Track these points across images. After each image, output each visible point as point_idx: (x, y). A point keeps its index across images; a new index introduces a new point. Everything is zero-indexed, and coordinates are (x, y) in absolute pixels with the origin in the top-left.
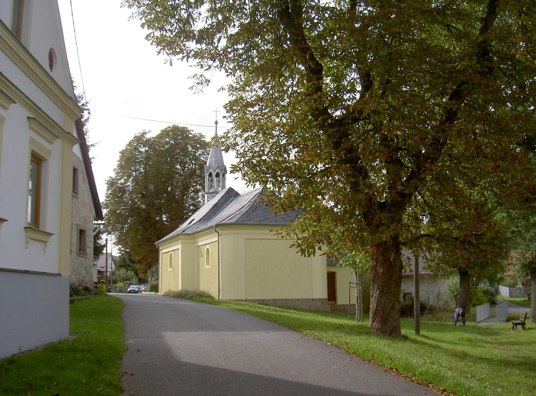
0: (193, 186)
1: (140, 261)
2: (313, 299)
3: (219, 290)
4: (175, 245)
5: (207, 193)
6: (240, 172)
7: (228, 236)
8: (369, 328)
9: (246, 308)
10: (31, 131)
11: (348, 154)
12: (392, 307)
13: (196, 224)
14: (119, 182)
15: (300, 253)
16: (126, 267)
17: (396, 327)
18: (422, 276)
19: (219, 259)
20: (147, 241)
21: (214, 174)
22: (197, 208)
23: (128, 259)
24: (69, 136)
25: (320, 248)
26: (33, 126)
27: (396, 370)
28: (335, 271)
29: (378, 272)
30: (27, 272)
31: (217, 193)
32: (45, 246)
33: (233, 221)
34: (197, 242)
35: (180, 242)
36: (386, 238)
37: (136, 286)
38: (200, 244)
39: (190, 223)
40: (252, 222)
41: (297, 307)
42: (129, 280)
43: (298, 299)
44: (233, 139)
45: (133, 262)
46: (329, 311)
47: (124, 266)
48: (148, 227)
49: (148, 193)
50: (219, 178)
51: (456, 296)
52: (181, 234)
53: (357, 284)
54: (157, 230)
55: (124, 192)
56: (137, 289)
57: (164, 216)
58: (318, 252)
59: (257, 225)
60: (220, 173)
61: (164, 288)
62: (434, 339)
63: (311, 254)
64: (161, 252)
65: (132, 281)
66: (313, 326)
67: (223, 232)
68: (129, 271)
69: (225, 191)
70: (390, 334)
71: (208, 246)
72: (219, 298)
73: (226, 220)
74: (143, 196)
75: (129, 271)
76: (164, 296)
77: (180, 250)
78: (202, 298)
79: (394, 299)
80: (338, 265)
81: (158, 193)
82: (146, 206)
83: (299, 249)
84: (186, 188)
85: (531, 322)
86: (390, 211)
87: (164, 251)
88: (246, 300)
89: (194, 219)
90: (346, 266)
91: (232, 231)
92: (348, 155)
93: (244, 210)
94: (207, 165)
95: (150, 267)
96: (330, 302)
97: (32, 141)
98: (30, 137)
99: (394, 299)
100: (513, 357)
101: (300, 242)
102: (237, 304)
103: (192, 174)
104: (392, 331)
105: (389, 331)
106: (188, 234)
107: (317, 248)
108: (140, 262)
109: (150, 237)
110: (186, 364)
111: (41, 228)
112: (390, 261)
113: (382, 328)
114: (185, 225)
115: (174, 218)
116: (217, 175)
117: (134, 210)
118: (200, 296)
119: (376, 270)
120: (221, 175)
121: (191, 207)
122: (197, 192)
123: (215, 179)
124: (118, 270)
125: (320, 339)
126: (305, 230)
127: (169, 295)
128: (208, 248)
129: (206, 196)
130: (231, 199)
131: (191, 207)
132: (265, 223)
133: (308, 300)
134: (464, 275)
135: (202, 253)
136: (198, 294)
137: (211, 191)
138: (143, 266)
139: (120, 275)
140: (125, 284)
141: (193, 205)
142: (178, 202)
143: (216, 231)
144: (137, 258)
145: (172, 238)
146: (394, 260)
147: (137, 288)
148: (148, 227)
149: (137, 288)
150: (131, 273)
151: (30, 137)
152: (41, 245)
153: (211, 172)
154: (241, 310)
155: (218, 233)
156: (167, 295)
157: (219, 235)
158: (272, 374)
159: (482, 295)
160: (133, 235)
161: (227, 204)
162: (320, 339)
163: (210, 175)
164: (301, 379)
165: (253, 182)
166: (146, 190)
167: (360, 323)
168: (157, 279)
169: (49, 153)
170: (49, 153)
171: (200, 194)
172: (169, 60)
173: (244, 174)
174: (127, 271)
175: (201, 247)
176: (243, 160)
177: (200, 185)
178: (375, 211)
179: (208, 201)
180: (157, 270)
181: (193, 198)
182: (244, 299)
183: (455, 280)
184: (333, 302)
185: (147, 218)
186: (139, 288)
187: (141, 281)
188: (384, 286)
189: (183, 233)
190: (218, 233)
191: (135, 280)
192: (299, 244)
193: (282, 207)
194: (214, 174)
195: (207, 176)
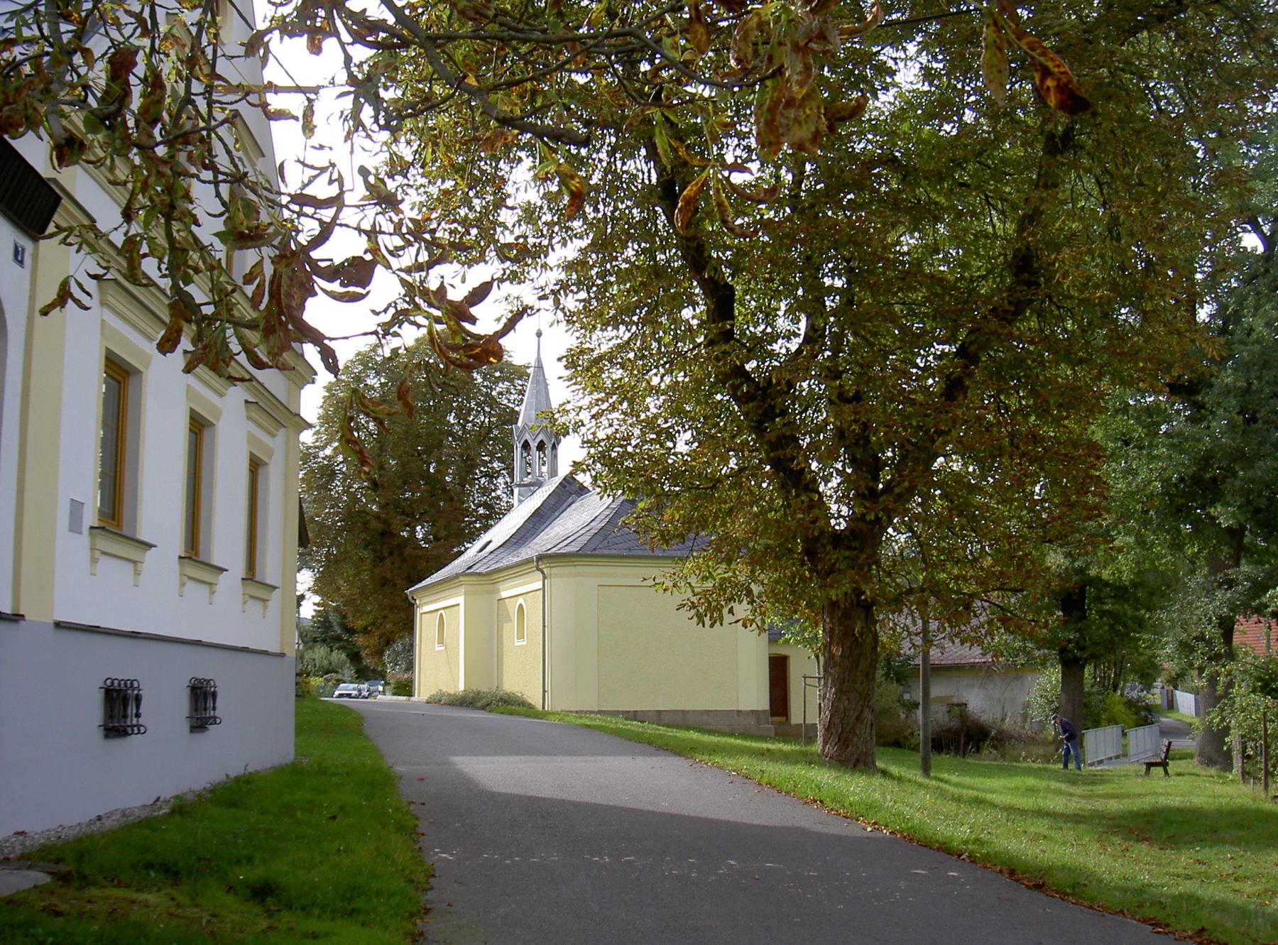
0: (485, 464)
1: (365, 628)
2: (739, 712)
3: (544, 691)
4: (450, 597)
5: (519, 486)
6: (588, 473)
7: (564, 580)
8: (818, 755)
9: (597, 723)
10: (250, 423)
11: (772, 451)
12: (858, 718)
13: (496, 553)
14: (321, 454)
15: (695, 619)
16: (328, 641)
17: (866, 754)
18: (989, 667)
19: (544, 626)
20: (384, 585)
21: (533, 445)
22: (494, 513)
23: (338, 623)
24: (297, 418)
25: (731, 611)
26: (253, 414)
27: (821, 801)
28: (787, 654)
29: (834, 655)
30: (245, 650)
31: (539, 484)
32: (265, 608)
33: (574, 548)
34: (499, 591)
35: (462, 589)
36: (837, 595)
37: (352, 686)
38: (504, 594)
39: (481, 550)
40: (615, 552)
41: (705, 727)
42: (336, 672)
43: (708, 712)
44: (574, 413)
45: (351, 631)
46: (773, 735)
47: (324, 641)
48: (386, 555)
49: (385, 479)
50: (544, 453)
51: (1056, 710)
52: (464, 574)
53: (819, 678)
54: (404, 560)
55: (332, 475)
56: (354, 693)
57: (418, 528)
58: (728, 618)
59: (623, 557)
60: (546, 441)
61: (425, 687)
62: (957, 785)
63: (715, 622)
64: (419, 611)
65: (343, 675)
66: (714, 750)
67: (554, 571)
68: (335, 653)
69: (557, 481)
70: (855, 766)
71: (521, 600)
72: (544, 708)
73: (559, 546)
74: (375, 486)
75: (335, 653)
76: (428, 703)
77: (462, 607)
78: (509, 707)
79: (861, 703)
80: (781, 641)
81: (407, 479)
82: (382, 507)
83: (693, 612)
84: (468, 466)
85: (1197, 763)
86: (849, 548)
87: (426, 609)
88: (599, 712)
89: (490, 542)
90: (797, 642)
91: (572, 570)
92: (772, 455)
93: (597, 525)
94: (520, 424)
95: (389, 643)
96: (777, 719)
97: (251, 439)
98: (249, 432)
99: (861, 703)
100: (1080, 809)
101: (694, 599)
102: (581, 718)
103: (483, 435)
104: (858, 761)
105: (853, 761)
106: (480, 574)
107: (725, 611)
108: (365, 631)
109: (389, 575)
110: (500, 794)
111: (257, 578)
112: (854, 635)
113: (840, 756)
114: (472, 551)
115: (443, 533)
116: (541, 447)
117: (354, 517)
118: (505, 701)
119: (830, 651)
120: (549, 446)
121: (481, 511)
122: (492, 475)
123: (536, 454)
124: (311, 648)
125: (720, 768)
126: (707, 578)
127: (440, 701)
128: (521, 605)
129: (516, 491)
130: (570, 500)
131: (481, 511)
132: (640, 553)
133: (728, 713)
134: (1071, 665)
135: (508, 614)
136: (501, 699)
137: (527, 480)
138: (374, 640)
139: (314, 660)
140: (328, 681)
141: (485, 505)
142: (452, 499)
143: (538, 569)
144: (360, 623)
145: (445, 581)
146: (861, 634)
147: (354, 689)
148: (386, 555)
149: (354, 689)
150: (339, 656)
151: (249, 432)
152: (259, 605)
153: (526, 441)
154: (588, 726)
155: (543, 573)
156: (435, 701)
157: (544, 578)
158: (632, 804)
159: (1123, 710)
160: (352, 572)
161: (562, 509)
162: (720, 768)
163: (526, 446)
164: (675, 810)
165: (612, 490)
166: (382, 472)
167: (803, 749)
168: (410, 666)
169: (270, 453)
170: (270, 453)
171: (501, 480)
172: (462, 274)
173: (596, 476)
174: (332, 651)
175: (507, 601)
176: (592, 451)
177: (501, 460)
178: (824, 546)
179: (520, 501)
180: (410, 648)
181: (485, 491)
182: (596, 709)
183: (1053, 676)
184: (783, 719)
185: (383, 534)
186: (360, 690)
187: (362, 674)
188: (844, 679)
189: (469, 572)
190: (543, 573)
191: (349, 672)
192: (693, 603)
193: (663, 536)
194: (533, 445)
195: (519, 449)
